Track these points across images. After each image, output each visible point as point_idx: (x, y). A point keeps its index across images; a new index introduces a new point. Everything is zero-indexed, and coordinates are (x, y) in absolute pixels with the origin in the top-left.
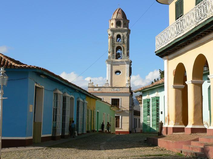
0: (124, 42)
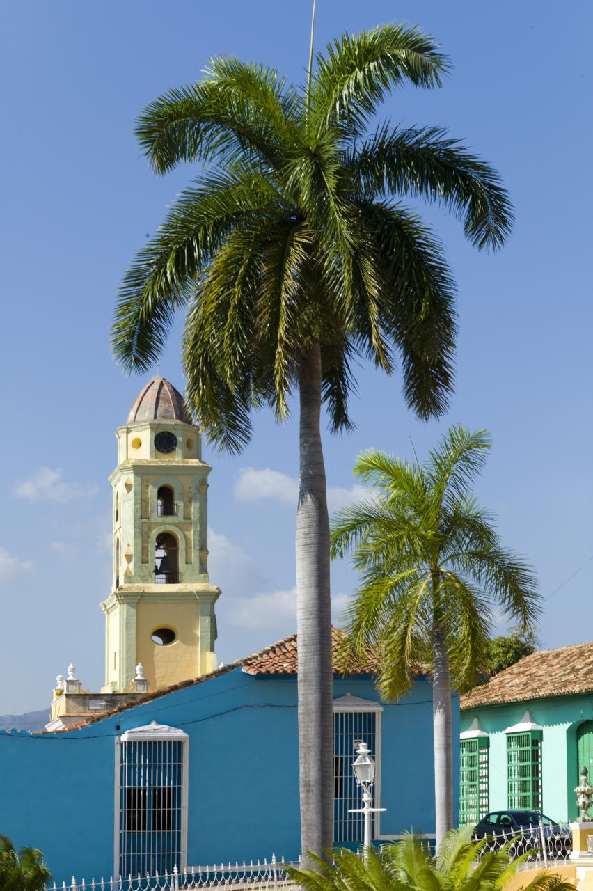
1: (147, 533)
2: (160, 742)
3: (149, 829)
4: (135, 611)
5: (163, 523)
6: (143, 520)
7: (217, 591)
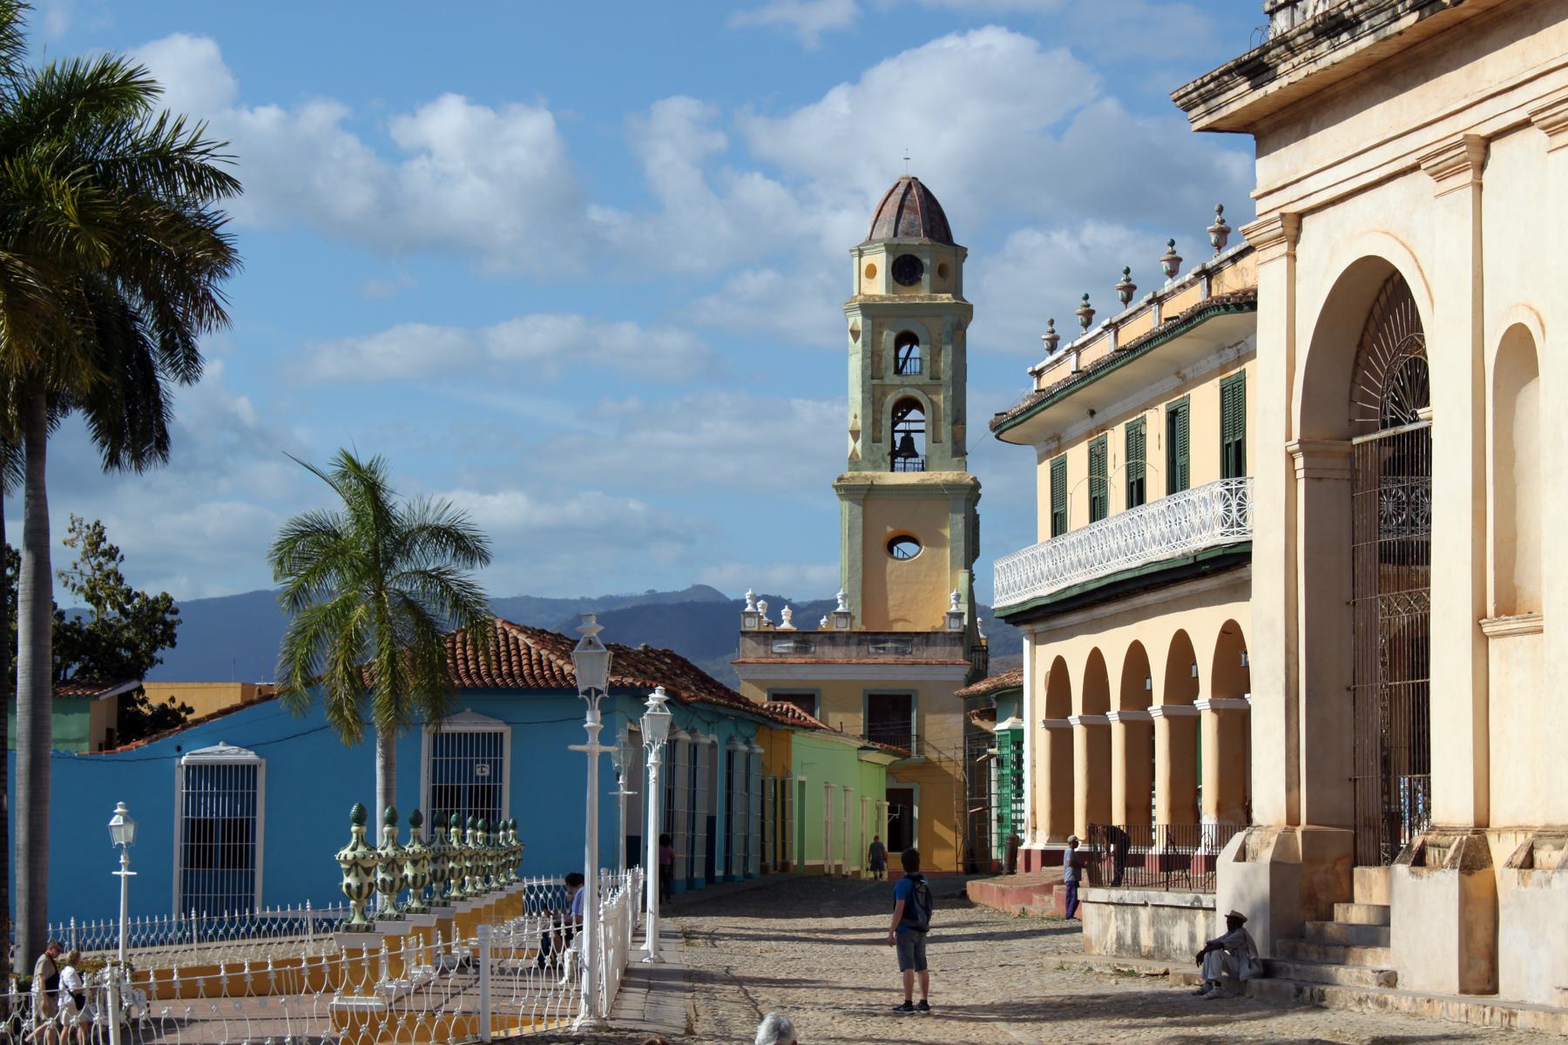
0: (935, 376)
1: (880, 399)
2: (225, 767)
3: (216, 866)
4: (861, 509)
5: (902, 386)
6: (875, 382)
7: (972, 482)
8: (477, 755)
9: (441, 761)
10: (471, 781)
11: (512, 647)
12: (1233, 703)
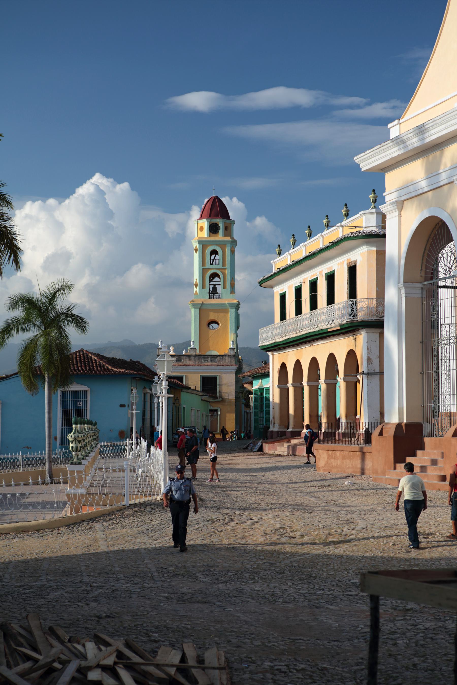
8: (78, 399)
9: (65, 401)
10: (76, 408)
11: (90, 360)
12: (332, 381)
